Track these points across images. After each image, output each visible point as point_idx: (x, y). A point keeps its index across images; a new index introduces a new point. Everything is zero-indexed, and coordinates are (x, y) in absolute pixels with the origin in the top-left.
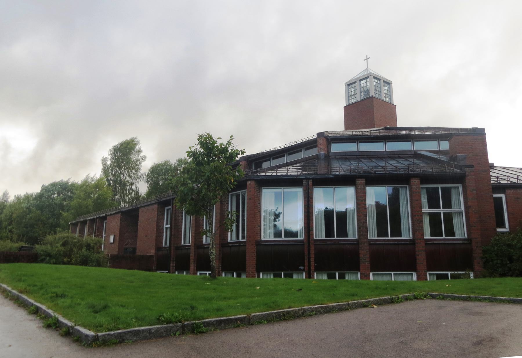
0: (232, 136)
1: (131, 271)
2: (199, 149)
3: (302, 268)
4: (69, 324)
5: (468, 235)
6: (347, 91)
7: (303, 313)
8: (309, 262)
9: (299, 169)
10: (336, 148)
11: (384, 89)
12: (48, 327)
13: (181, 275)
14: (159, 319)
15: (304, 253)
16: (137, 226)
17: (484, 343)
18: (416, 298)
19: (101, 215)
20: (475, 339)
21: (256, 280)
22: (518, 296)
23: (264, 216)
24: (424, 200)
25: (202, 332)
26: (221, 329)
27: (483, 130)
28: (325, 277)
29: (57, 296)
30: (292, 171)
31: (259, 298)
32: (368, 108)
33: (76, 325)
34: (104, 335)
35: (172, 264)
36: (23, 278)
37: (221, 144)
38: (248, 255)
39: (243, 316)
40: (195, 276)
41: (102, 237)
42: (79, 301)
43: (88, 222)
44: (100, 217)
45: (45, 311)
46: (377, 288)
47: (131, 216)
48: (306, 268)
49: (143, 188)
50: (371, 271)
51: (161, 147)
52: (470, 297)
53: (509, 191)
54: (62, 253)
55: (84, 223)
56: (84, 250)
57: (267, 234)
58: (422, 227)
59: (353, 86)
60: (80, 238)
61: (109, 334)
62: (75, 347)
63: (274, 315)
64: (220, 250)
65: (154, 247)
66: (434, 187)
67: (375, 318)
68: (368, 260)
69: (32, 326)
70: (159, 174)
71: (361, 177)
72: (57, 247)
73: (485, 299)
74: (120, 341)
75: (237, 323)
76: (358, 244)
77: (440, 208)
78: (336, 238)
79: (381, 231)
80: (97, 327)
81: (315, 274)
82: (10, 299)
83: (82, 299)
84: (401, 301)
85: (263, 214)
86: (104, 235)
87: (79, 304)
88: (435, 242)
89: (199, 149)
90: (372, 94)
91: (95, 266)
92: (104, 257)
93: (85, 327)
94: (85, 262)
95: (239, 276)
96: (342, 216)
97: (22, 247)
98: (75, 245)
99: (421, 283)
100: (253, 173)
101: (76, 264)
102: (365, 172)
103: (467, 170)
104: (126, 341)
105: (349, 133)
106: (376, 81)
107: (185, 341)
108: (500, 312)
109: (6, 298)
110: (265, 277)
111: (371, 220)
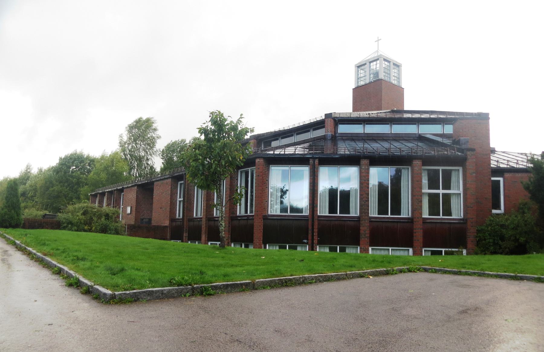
0: (242, 115)
1: (147, 239)
2: (210, 126)
3: (305, 241)
4: (89, 283)
5: (464, 215)
6: (357, 73)
7: (303, 281)
8: (313, 236)
9: (306, 148)
10: (343, 129)
11: (394, 72)
12: (70, 285)
13: (193, 244)
14: (170, 282)
15: (308, 228)
16: (152, 198)
17: (469, 312)
18: (410, 271)
19: (119, 188)
20: (461, 308)
21: (262, 250)
22: (505, 272)
23: (272, 193)
24: (425, 181)
25: (210, 295)
26: (228, 292)
27: (487, 115)
28: (327, 250)
29: (78, 259)
30: (299, 150)
31: (264, 267)
32: (376, 92)
33: (95, 285)
34: (120, 294)
35: (185, 235)
36: (47, 243)
37: (232, 122)
38: (255, 231)
39: (247, 281)
40: (206, 245)
41: (120, 207)
42: (98, 264)
43: (106, 194)
44: (117, 190)
45: (67, 272)
46: (374, 261)
47: (146, 189)
48: (310, 242)
49: (157, 163)
50: (371, 246)
51: (180, 126)
52: (460, 272)
53: (507, 175)
54: (82, 221)
55: (103, 194)
56: (103, 219)
57: (274, 209)
58: (421, 207)
59: (363, 67)
60: (100, 208)
61: (125, 294)
62: (94, 303)
63: (277, 281)
64: (229, 223)
65: (168, 218)
66: (435, 170)
67: (370, 288)
68: (368, 235)
69: (56, 284)
70: (173, 151)
71: (365, 157)
72: (78, 216)
73: (474, 274)
74: (135, 299)
75: (242, 287)
76: (359, 221)
77: (439, 189)
78: (338, 214)
79: (382, 209)
80: (114, 287)
81: (318, 247)
82: (35, 261)
83: (101, 262)
84: (396, 274)
85: (270, 190)
86: (122, 207)
87: (98, 267)
88: (432, 221)
89: (210, 126)
90: (382, 76)
91: (114, 234)
92: (122, 226)
93: (103, 286)
94: (104, 230)
95: (247, 246)
96: (346, 195)
97: (46, 215)
98: (95, 214)
99: (416, 258)
100: (262, 151)
101: (96, 231)
102: (369, 152)
103: (469, 153)
104: (141, 300)
105: (356, 115)
106: (386, 63)
107: (194, 301)
108: (487, 285)
109: (32, 259)
110: (271, 248)
111: (372, 199)
